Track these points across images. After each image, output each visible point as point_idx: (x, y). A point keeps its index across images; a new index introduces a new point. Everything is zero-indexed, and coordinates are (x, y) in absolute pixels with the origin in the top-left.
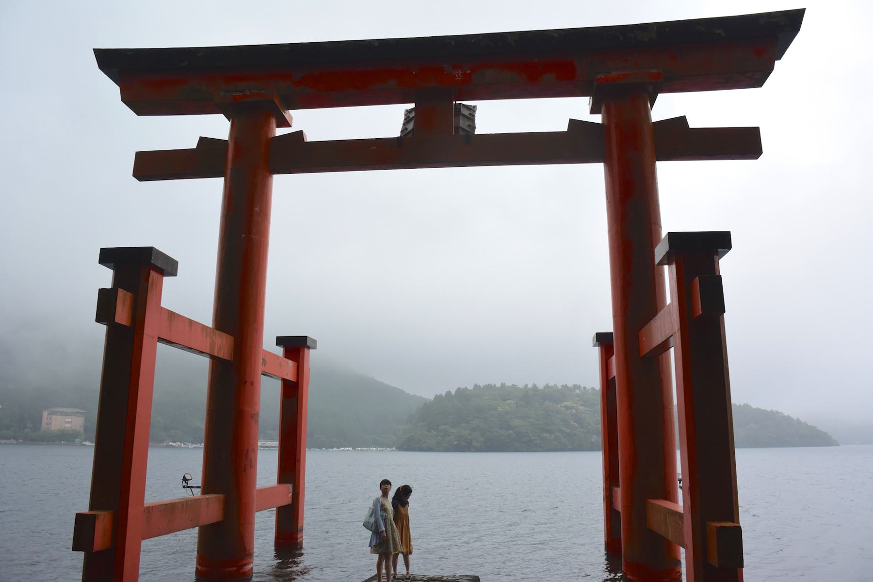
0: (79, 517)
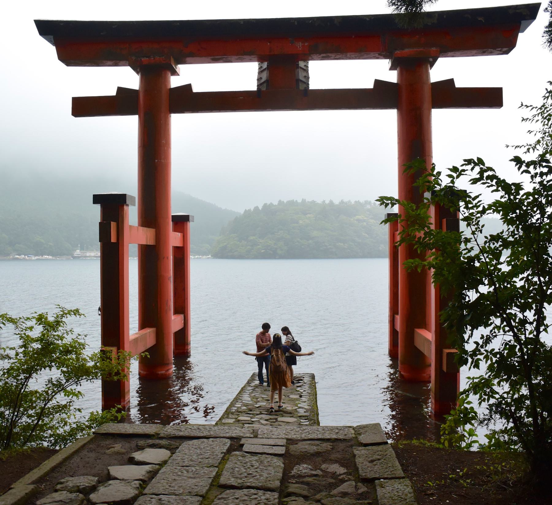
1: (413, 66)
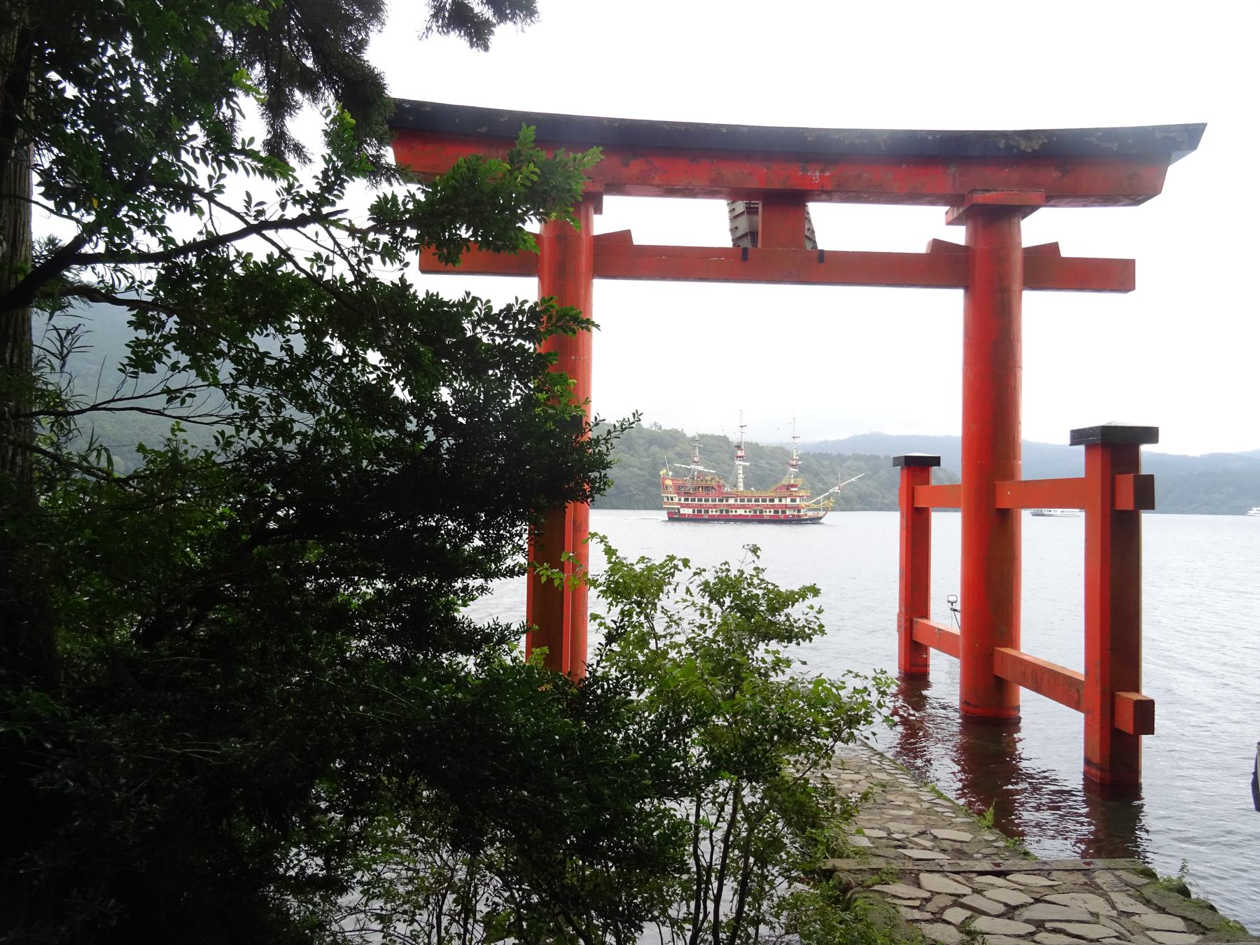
0: (1151, 731)
1: (994, 219)
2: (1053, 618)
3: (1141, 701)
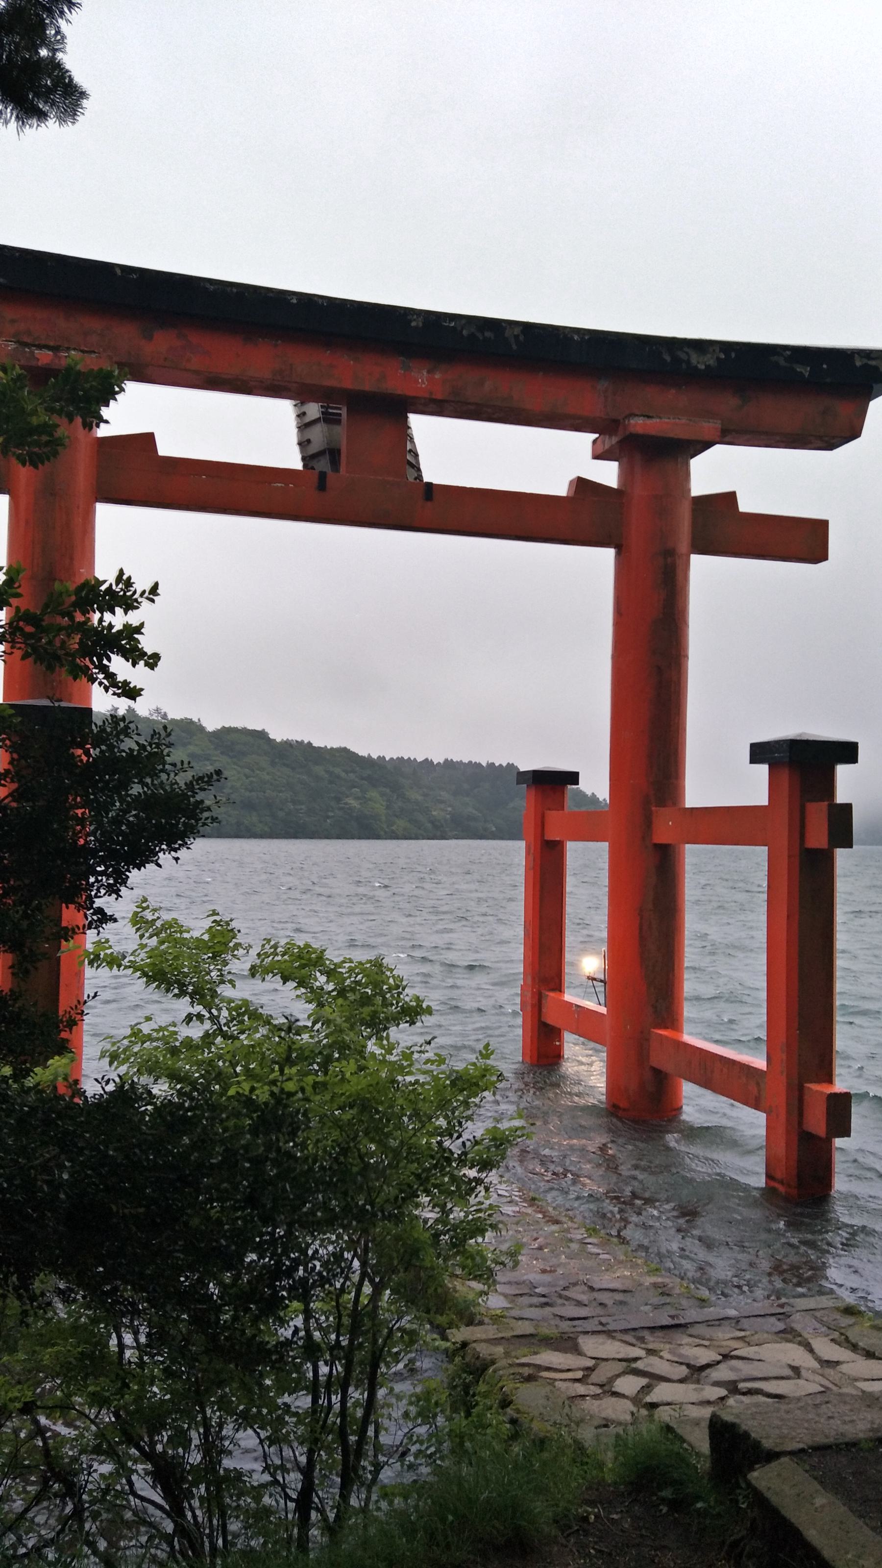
1: (656, 456)
2: (726, 994)
3: (836, 1095)
